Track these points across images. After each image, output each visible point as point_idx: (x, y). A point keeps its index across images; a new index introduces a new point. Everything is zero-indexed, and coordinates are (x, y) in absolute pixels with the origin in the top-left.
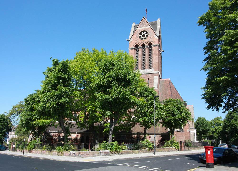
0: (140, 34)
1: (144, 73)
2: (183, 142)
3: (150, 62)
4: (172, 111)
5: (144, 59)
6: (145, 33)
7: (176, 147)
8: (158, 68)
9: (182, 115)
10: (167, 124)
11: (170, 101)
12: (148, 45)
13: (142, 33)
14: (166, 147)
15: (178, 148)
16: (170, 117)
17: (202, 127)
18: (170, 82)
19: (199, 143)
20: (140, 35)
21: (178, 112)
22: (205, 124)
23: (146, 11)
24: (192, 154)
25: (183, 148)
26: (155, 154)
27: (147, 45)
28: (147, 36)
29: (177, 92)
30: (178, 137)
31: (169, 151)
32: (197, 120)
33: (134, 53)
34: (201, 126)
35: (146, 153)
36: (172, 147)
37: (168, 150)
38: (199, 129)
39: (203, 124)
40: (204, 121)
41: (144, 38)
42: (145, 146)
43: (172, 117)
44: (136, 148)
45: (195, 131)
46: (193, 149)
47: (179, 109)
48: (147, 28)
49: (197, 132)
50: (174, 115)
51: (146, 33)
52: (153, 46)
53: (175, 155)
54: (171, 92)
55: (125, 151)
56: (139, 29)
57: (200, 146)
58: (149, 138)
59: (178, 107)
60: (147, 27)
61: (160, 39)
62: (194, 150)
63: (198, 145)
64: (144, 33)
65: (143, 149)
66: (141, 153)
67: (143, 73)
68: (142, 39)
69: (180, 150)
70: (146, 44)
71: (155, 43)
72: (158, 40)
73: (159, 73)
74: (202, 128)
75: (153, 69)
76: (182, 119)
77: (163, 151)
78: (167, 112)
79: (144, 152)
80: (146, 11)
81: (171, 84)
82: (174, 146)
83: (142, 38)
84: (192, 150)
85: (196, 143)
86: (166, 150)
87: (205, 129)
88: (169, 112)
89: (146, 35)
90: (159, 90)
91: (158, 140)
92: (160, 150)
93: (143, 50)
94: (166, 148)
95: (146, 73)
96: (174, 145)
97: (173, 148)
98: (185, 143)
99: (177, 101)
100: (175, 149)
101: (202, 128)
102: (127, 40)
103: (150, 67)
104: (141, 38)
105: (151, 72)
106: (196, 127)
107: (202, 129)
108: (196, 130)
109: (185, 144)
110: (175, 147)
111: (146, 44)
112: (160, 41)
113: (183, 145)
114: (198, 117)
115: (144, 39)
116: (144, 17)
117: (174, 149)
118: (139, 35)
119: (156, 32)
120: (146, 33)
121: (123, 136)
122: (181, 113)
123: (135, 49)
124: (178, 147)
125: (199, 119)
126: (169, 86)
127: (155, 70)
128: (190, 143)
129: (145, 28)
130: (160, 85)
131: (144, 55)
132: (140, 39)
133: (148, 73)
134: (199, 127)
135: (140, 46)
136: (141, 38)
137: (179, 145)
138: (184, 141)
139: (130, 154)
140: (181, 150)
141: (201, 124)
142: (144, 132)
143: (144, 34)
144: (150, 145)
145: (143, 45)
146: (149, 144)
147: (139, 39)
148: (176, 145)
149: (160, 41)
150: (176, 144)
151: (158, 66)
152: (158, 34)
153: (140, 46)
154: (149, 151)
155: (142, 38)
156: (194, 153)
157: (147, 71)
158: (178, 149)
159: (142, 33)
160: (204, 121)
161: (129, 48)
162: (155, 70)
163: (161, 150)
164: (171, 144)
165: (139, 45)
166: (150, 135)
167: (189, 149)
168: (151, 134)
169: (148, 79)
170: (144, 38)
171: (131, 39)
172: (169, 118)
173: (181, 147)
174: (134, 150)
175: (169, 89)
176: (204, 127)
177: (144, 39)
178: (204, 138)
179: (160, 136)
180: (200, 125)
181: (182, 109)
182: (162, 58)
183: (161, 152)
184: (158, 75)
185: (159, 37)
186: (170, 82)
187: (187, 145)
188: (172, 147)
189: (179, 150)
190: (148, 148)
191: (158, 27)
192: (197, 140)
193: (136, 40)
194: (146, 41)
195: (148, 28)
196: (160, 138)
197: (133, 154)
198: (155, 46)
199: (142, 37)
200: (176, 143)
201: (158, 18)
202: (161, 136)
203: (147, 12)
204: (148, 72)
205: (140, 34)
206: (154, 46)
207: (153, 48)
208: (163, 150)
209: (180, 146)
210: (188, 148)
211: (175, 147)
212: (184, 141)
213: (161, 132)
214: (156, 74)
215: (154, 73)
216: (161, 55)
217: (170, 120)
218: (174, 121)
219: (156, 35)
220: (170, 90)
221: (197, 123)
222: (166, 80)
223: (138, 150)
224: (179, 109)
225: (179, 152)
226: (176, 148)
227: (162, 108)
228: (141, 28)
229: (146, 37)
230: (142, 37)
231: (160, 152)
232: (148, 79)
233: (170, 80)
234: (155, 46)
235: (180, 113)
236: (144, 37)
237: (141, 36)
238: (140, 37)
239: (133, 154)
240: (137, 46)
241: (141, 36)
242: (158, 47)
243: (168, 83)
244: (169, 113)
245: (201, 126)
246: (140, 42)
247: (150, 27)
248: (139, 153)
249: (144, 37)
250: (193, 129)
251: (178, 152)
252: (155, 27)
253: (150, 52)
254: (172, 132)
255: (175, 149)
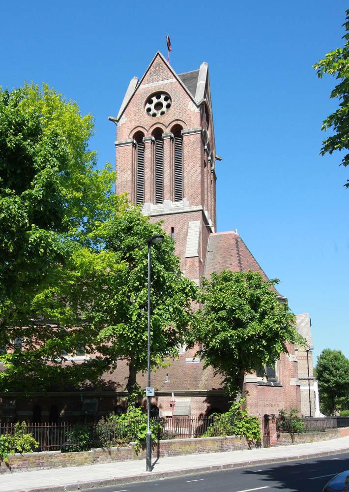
0: (149, 101)
1: (160, 213)
2: (273, 416)
3: (178, 180)
4: (232, 311)
5: (159, 172)
6: (163, 97)
7: (248, 435)
8: (200, 196)
9: (266, 321)
10: (218, 356)
11: (226, 279)
12: (172, 131)
13: (152, 99)
14: (212, 435)
15: (255, 438)
16: (224, 330)
17: (334, 376)
18: (237, 241)
19: (325, 418)
20: (148, 106)
21: (249, 312)
22: (341, 367)
23: (169, 44)
24: (303, 456)
25: (274, 436)
26: (150, 466)
27: (167, 131)
28: (168, 106)
29: (251, 261)
30: (257, 398)
31: (222, 450)
32: (322, 358)
33: (131, 155)
34: (331, 373)
35: (86, 467)
36: (233, 433)
37: (219, 444)
38: (328, 381)
39: (337, 369)
40: (339, 359)
41: (158, 113)
42: (124, 435)
43: (233, 332)
44: (81, 440)
45: (315, 386)
46: (308, 439)
47: (255, 303)
48: (166, 82)
49: (322, 390)
50: (239, 324)
51: (166, 99)
52: (185, 133)
53: (235, 465)
54: (239, 268)
55: (28, 457)
56: (149, 87)
57: (329, 427)
58: (171, 405)
59: (252, 295)
60: (166, 82)
61: (208, 120)
62: (311, 441)
63: (325, 426)
64: (158, 98)
65: (114, 444)
66: (104, 460)
67: (158, 212)
68: (154, 115)
69: (262, 443)
70: (167, 128)
71: (190, 125)
72: (199, 116)
73: (202, 211)
74: (335, 379)
75: (185, 199)
76: (264, 336)
77: (200, 451)
78: (217, 314)
79: (119, 458)
80: (169, 44)
81: (239, 244)
82: (241, 430)
83: (155, 111)
84: (304, 442)
85: (317, 420)
86: (210, 445)
87: (343, 381)
88: (223, 313)
89: (165, 103)
90: (207, 264)
91: (198, 415)
92: (187, 447)
93: (157, 149)
94: (213, 440)
95: (164, 213)
96: (243, 426)
97: (239, 436)
98: (282, 419)
99: (250, 278)
100: (245, 439)
101: (335, 379)
102: (110, 119)
103: (178, 196)
104: (151, 113)
105: (180, 209)
106: (320, 375)
107: (336, 382)
108: (319, 386)
109: (283, 425)
110: (244, 434)
111: (167, 128)
112: (210, 126)
113: (272, 426)
114: (323, 349)
115: (159, 115)
116: (158, 53)
117: (240, 441)
118: (145, 105)
119: (194, 97)
120: (166, 99)
121: (88, 401)
122: (263, 314)
123: (134, 145)
124: (255, 433)
125: (326, 354)
126: (235, 251)
127: (192, 204)
128: (299, 420)
129: (162, 82)
130: (208, 249)
131: (159, 161)
132: (149, 115)
133: (173, 212)
134: (328, 377)
135: (148, 135)
136: (151, 113)
137: (262, 426)
138: (277, 414)
139: (53, 471)
140: (268, 444)
141: (332, 369)
142: (127, 380)
143: (158, 100)
144: (144, 429)
145: (158, 133)
146: (142, 425)
147: (147, 116)
148: (247, 428)
149: (209, 128)
150: (247, 425)
151: (199, 191)
152: (199, 97)
153: (148, 135)
154: (140, 454)
155: (155, 111)
156: (309, 456)
157: (169, 205)
158: (257, 442)
159: (152, 99)
160: (339, 359)
161: (116, 143)
162: (192, 204)
163: (193, 446)
164: (232, 423)
165: (145, 132)
166: (173, 398)
167: (296, 439)
168: (177, 394)
169: (173, 229)
170: (158, 113)
171: (124, 116)
172: (221, 335)
173: (267, 433)
174: (76, 451)
175: (233, 258)
176: (340, 376)
177: (159, 115)
178: (340, 407)
179: (205, 398)
180: (329, 370)
181: (266, 303)
182: (215, 178)
183: (193, 456)
184: (201, 217)
185: (204, 108)
186: (239, 240)
187: (289, 426)
188: (234, 436)
189: (258, 445)
190: (136, 443)
191: (201, 83)
192: (323, 412)
193: (134, 118)
194: (166, 121)
195: (171, 84)
196: (204, 407)
197: (69, 469)
198: (192, 132)
199: (153, 111)
200: (247, 422)
201: (201, 63)
202: (206, 401)
203: (171, 49)
204: (171, 210)
205: (149, 101)
206: (188, 133)
207: (186, 139)
208: (198, 445)
209: (262, 431)
210: (292, 437)
211: (244, 434)
212: (277, 414)
213: (206, 386)
214: (194, 213)
215: (189, 210)
216: (213, 168)
217: (224, 342)
218: (238, 346)
219: (192, 103)
220: (237, 263)
221: (320, 365)
222: (225, 236)
223: (92, 451)
224: (255, 303)
225: (261, 450)
226: (250, 439)
227: (187, 290)
228: (150, 85)
229: (164, 109)
230: (153, 111)
231: (185, 454)
232: (173, 229)
233: (237, 233)
234: (192, 132)
235: (258, 315)
236: (160, 111)
237: (152, 106)
238: (149, 110)
239: (65, 466)
240: (139, 136)
241: (152, 106)
242: (199, 136)
243: (233, 242)
244: (223, 319)
245: (331, 373)
246: (147, 124)
247: (175, 80)
248: (95, 461)
249: (160, 111)
250: (309, 379)
251: (255, 450)
252: (194, 85)
253: (178, 149)
254: (238, 383)
255: (246, 443)
